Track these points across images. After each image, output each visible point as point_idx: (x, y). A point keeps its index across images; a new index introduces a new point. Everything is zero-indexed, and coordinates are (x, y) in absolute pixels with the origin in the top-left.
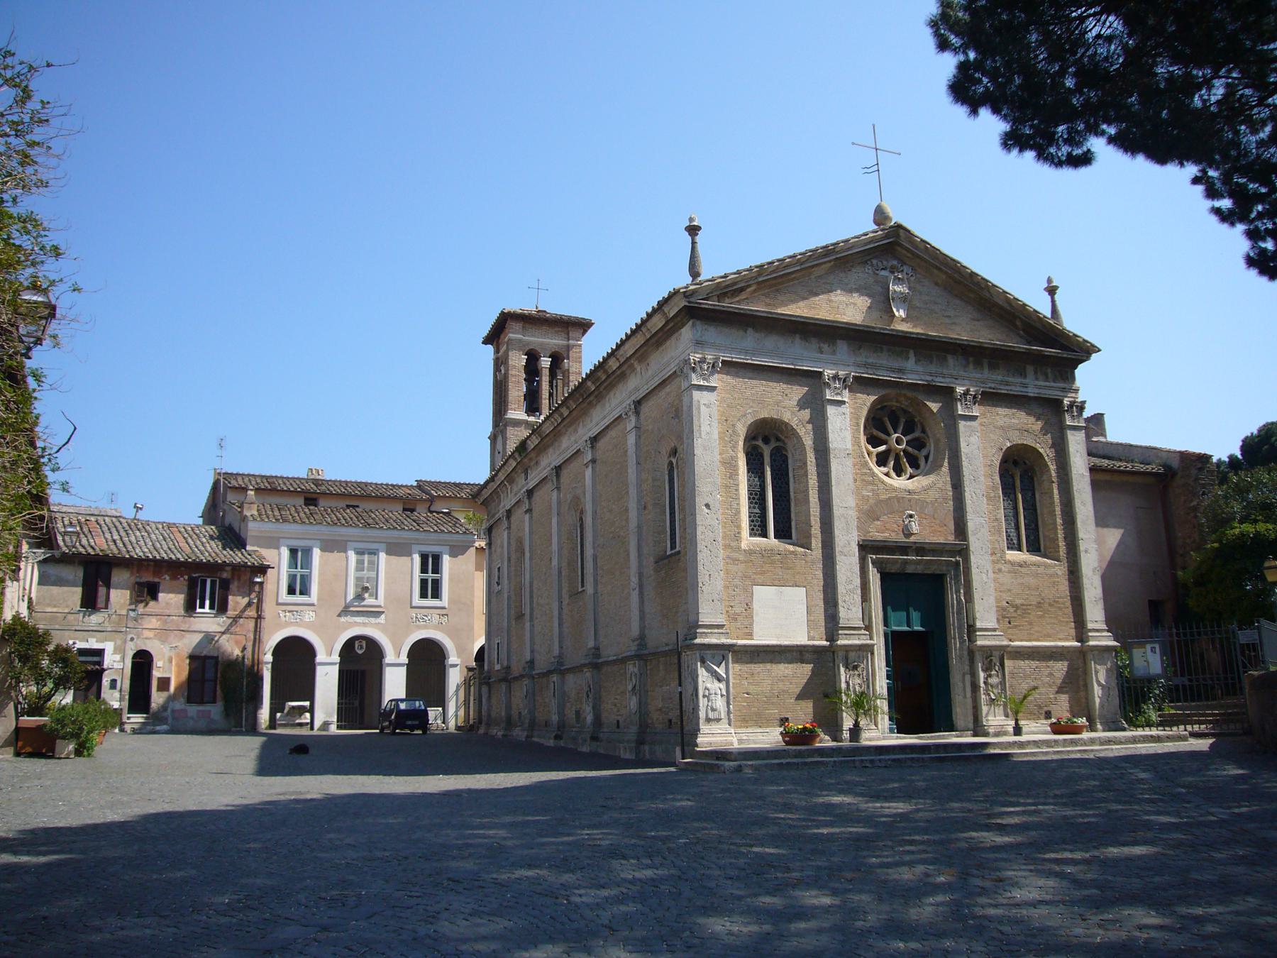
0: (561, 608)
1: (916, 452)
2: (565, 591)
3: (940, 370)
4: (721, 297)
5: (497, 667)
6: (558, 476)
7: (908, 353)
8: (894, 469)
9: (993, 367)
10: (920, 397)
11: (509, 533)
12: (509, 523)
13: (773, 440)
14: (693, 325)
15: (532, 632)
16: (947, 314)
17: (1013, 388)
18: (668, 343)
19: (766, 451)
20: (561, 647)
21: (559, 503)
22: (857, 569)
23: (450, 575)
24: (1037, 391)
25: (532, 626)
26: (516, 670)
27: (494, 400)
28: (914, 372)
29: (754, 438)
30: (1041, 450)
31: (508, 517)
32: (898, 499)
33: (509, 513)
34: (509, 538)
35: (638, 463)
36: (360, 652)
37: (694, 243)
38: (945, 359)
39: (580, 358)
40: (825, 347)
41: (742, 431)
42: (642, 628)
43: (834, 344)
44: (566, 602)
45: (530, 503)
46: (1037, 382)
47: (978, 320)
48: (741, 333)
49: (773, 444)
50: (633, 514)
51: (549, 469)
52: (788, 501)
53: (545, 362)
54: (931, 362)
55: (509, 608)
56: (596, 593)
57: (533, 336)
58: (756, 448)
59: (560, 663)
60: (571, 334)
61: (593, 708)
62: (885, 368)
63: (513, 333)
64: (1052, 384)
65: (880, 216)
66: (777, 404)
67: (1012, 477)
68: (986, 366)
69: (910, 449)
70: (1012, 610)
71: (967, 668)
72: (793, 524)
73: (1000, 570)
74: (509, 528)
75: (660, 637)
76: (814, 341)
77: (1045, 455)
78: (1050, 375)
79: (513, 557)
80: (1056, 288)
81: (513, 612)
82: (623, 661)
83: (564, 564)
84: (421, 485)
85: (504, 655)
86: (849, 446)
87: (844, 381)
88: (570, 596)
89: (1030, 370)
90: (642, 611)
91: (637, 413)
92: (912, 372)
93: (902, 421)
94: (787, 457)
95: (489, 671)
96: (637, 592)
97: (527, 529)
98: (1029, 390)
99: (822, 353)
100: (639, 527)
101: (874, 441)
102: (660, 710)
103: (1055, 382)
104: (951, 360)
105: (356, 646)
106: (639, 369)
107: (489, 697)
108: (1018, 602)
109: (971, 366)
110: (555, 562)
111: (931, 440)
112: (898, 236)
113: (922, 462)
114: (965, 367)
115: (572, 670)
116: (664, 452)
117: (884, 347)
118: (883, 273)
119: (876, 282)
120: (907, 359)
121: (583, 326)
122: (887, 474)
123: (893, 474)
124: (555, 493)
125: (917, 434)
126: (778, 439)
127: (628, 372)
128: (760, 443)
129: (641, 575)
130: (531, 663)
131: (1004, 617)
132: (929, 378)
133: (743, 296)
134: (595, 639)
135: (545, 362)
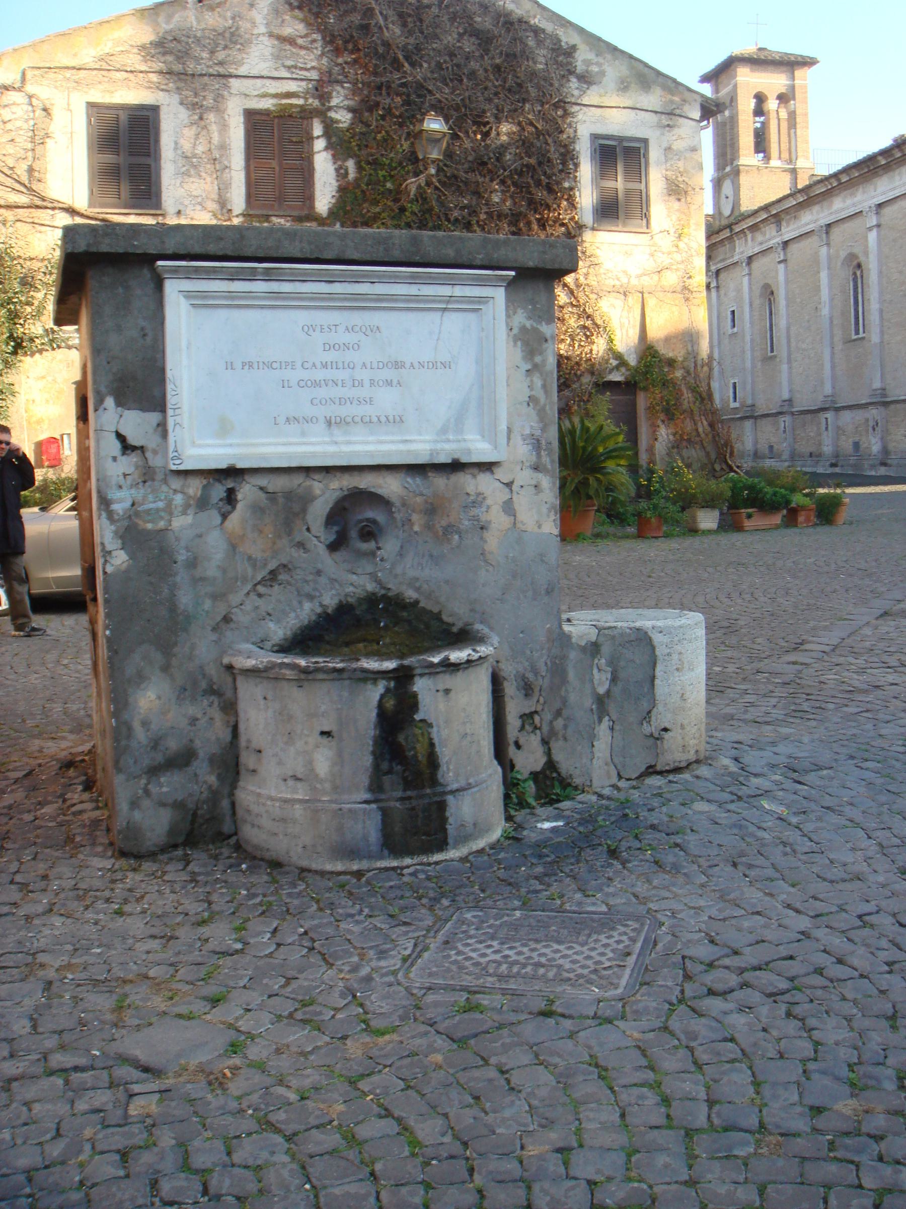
0: (833, 354)
11: (750, 280)
12: (750, 270)
15: (790, 373)
25: (790, 368)
74: (750, 274)
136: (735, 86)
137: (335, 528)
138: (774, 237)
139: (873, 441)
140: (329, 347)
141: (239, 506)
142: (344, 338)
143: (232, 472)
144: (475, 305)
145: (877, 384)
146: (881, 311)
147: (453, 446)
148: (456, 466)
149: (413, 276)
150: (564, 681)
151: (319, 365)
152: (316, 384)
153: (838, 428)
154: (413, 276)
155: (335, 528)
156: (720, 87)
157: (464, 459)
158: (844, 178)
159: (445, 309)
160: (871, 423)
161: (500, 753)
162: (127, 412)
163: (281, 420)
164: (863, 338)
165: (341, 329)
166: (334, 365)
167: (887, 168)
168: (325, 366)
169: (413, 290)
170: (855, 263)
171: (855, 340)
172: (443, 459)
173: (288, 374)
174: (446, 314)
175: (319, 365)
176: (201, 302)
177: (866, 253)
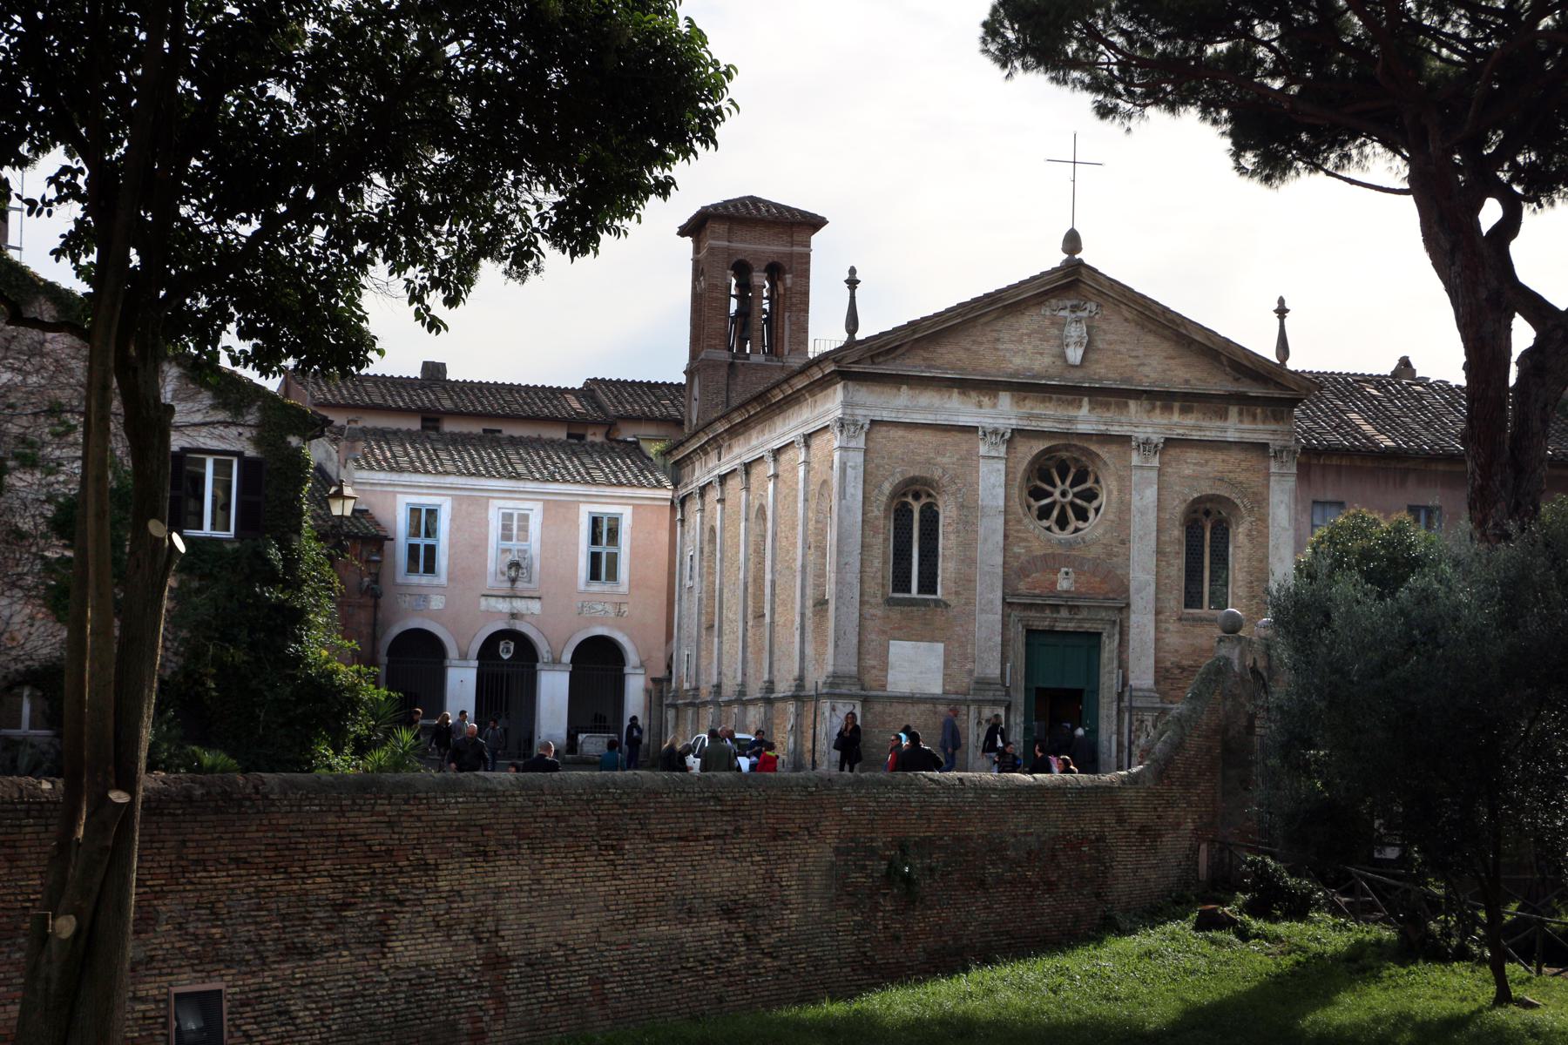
0: (745, 630)
1: (1085, 504)
2: (750, 610)
3: (1117, 417)
4: (873, 359)
5: (686, 686)
6: (747, 473)
7: (1081, 401)
8: (1078, 519)
9: (1185, 411)
10: (1094, 448)
11: (702, 517)
12: (703, 504)
14: (845, 387)
15: (720, 649)
16: (1134, 354)
17: (1208, 433)
19: (916, 508)
20: (744, 674)
21: (748, 506)
22: (999, 627)
23: (632, 548)
24: (1237, 435)
25: (721, 643)
26: (705, 693)
27: (692, 319)
28: (1086, 419)
29: (905, 495)
30: (1238, 501)
31: (702, 496)
32: (1054, 556)
33: (703, 490)
34: (702, 523)
35: (806, 500)
36: (506, 657)
37: (853, 298)
38: (1126, 405)
39: (808, 270)
40: (986, 400)
41: (887, 487)
42: (802, 669)
43: (996, 396)
44: (750, 623)
45: (722, 492)
46: (1243, 426)
47: (1173, 358)
48: (895, 391)
49: (924, 500)
50: (799, 551)
51: (738, 461)
54: (1108, 410)
55: (700, 613)
56: (772, 622)
57: (742, 241)
58: (905, 504)
59: (742, 693)
60: (795, 238)
62: (1049, 416)
63: (713, 239)
64: (1261, 427)
65: (1072, 241)
66: (929, 461)
69: (1078, 501)
71: (1114, 728)
72: (939, 579)
73: (1167, 630)
74: (702, 510)
76: (973, 394)
77: (1241, 506)
78: (1259, 416)
79: (706, 549)
80: (1288, 311)
81: (703, 619)
82: (784, 699)
83: (750, 580)
84: (593, 389)
85: (693, 672)
86: (1001, 503)
87: (1003, 435)
89: (1233, 411)
91: (807, 446)
92: (1084, 422)
93: (1073, 471)
94: (937, 513)
95: (677, 691)
97: (718, 523)
99: (981, 407)
100: (804, 567)
101: (1037, 494)
103: (1264, 423)
104: (1132, 404)
105: (501, 647)
107: (676, 726)
108: (1185, 663)
109: (1158, 411)
110: (741, 576)
111: (1105, 492)
112: (1080, 274)
113: (1091, 515)
114: (1149, 411)
115: (753, 702)
117: (1054, 396)
118: (1062, 313)
119: (1052, 323)
120: (1080, 407)
121: (816, 223)
122: (1049, 529)
123: (1055, 528)
124: (744, 493)
125: (1089, 484)
126: (929, 495)
128: (910, 499)
129: (803, 615)
130: (718, 687)
131: (1166, 678)
132: (1103, 428)
133: (899, 351)
134: (770, 672)
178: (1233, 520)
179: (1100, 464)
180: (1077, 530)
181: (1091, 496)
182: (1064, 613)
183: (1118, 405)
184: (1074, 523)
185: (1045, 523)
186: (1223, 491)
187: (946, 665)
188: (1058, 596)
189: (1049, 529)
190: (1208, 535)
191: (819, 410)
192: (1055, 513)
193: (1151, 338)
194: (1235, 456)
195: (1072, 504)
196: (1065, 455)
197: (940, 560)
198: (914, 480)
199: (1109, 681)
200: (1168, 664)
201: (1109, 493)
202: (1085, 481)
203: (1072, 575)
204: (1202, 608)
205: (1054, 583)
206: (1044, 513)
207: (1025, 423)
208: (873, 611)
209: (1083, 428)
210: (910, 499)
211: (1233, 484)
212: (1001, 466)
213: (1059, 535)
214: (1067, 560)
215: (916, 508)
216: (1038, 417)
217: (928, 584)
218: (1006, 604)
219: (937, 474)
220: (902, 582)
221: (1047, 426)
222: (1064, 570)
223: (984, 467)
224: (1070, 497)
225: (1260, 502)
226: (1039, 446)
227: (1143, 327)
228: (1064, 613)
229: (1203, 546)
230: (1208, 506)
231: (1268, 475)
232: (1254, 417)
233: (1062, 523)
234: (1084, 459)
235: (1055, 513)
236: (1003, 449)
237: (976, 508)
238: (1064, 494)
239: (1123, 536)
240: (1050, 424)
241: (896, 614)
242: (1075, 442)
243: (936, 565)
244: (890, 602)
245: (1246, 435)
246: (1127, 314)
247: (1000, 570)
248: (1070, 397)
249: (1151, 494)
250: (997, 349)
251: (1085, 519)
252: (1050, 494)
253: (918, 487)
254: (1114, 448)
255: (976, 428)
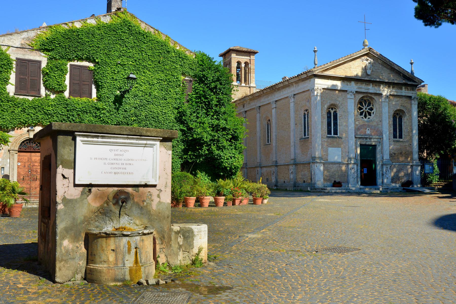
1: (370, 111)
7: (370, 84)
10: (373, 96)
13: (334, 109)
18: (306, 81)
19: (332, 112)
24: (405, 94)
29: (329, 109)
30: (405, 111)
40: (348, 83)
41: (326, 106)
43: (351, 82)
49: (334, 110)
52: (337, 125)
53: (243, 65)
58: (329, 111)
61: (276, 177)
62: (364, 88)
64: (410, 92)
67: (396, 118)
68: (391, 87)
69: (369, 111)
70: (393, 155)
72: (338, 131)
75: (301, 158)
76: (346, 82)
78: (409, 89)
88: (264, 145)
89: (403, 88)
90: (295, 152)
96: (293, 147)
98: (403, 94)
102: (301, 178)
106: (295, 85)
113: (372, 114)
116: (302, 110)
122: (362, 118)
125: (371, 106)
126: (335, 109)
127: (291, 85)
128: (330, 110)
131: (391, 156)
135: (243, 65)
136: (231, 58)
137: (115, 200)
138: (242, 109)
139: (273, 178)
140: (116, 155)
141: (92, 193)
142: (119, 152)
143: (91, 185)
144: (152, 146)
145: (274, 160)
146: (276, 135)
147: (146, 180)
148: (146, 186)
149: (137, 138)
150: (171, 240)
151: (113, 159)
152: (112, 164)
153: (262, 173)
154: (137, 138)
155: (115, 200)
156: (226, 58)
157: (148, 184)
158: (265, 92)
159: (145, 147)
160: (272, 172)
161: (155, 258)
162: (65, 169)
163: (103, 172)
164: (270, 144)
165: (119, 151)
166: (117, 160)
167: (279, 89)
168: (114, 159)
169: (137, 142)
170: (268, 119)
171: (267, 145)
172: (143, 183)
173: (105, 161)
174: (145, 148)
175: (113, 159)
176: (85, 142)
177: (271, 116)
178: (403, 116)
179: (374, 101)
180: (369, 118)
181: (372, 109)
182: (368, 140)
183: (378, 85)
184: (368, 117)
185: (362, 116)
186: (402, 108)
187: (342, 154)
188: (366, 135)
189: (362, 118)
190: (398, 120)
191: (306, 85)
192: (364, 114)
193: (385, 69)
194: (404, 99)
195: (368, 111)
196: (365, 98)
197: (338, 126)
198: (332, 105)
199: (378, 156)
200: (392, 153)
201: (376, 109)
202: (370, 106)
203: (370, 130)
204: (397, 138)
205: (366, 132)
206: (360, 109)
207: (358, 89)
208: (324, 140)
209: (371, 91)
210: (330, 110)
211: (404, 106)
212: (353, 101)
213: (366, 120)
214: (369, 126)
215: (332, 112)
216: (361, 88)
217: (336, 133)
218: (356, 137)
219: (338, 103)
220: (329, 133)
221: (363, 90)
222: (368, 128)
223: (349, 101)
224: (367, 110)
225: (410, 111)
226: (361, 96)
227: (383, 66)
228: (368, 140)
229: (396, 122)
230: (398, 112)
231: (411, 104)
232: (408, 89)
233: (365, 116)
234: (370, 100)
235: (364, 114)
236: (353, 96)
237: (347, 112)
238: (366, 109)
239: (380, 120)
240: (364, 90)
241: (330, 140)
242: (369, 95)
243: (337, 127)
244: (328, 137)
245: (407, 94)
246: (379, 62)
247: (354, 129)
248: (368, 83)
249: (387, 109)
250: (350, 70)
251: (371, 115)
252: (362, 109)
253: (332, 107)
254: (378, 97)
255: (347, 91)
